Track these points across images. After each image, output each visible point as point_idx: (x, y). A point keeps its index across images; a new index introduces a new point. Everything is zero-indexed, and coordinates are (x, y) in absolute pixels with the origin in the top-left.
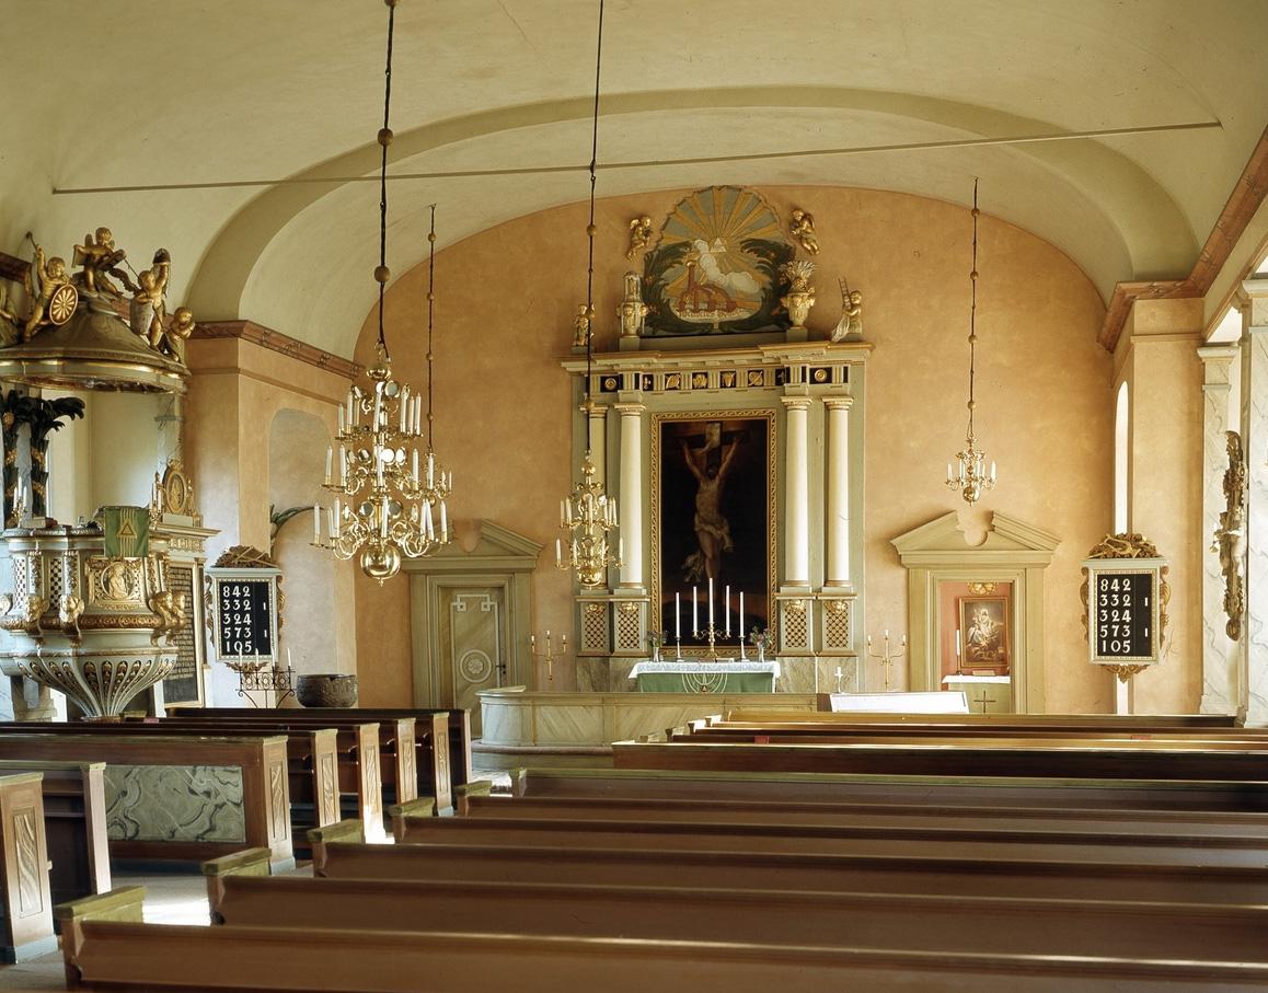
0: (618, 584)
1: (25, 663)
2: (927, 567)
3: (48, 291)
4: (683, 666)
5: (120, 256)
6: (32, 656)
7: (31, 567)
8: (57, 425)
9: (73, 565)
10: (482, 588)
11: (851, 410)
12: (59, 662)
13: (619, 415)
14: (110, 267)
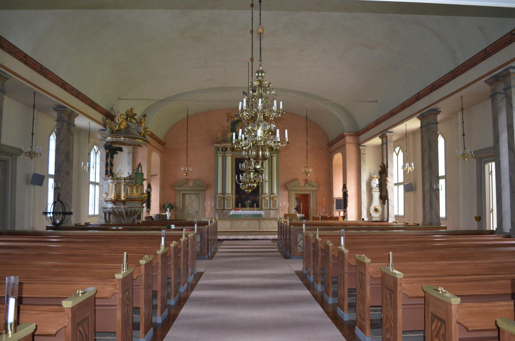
0: (225, 193)
1: (111, 210)
2: (293, 190)
3: (120, 122)
4: (240, 212)
5: (135, 115)
6: (113, 208)
7: (114, 187)
8: (117, 153)
9: (125, 186)
10: (193, 194)
11: (277, 157)
12: (120, 210)
13: (226, 156)
14: (133, 117)
